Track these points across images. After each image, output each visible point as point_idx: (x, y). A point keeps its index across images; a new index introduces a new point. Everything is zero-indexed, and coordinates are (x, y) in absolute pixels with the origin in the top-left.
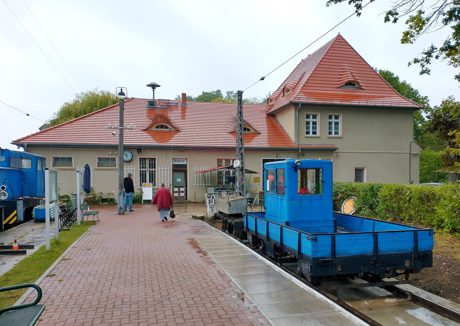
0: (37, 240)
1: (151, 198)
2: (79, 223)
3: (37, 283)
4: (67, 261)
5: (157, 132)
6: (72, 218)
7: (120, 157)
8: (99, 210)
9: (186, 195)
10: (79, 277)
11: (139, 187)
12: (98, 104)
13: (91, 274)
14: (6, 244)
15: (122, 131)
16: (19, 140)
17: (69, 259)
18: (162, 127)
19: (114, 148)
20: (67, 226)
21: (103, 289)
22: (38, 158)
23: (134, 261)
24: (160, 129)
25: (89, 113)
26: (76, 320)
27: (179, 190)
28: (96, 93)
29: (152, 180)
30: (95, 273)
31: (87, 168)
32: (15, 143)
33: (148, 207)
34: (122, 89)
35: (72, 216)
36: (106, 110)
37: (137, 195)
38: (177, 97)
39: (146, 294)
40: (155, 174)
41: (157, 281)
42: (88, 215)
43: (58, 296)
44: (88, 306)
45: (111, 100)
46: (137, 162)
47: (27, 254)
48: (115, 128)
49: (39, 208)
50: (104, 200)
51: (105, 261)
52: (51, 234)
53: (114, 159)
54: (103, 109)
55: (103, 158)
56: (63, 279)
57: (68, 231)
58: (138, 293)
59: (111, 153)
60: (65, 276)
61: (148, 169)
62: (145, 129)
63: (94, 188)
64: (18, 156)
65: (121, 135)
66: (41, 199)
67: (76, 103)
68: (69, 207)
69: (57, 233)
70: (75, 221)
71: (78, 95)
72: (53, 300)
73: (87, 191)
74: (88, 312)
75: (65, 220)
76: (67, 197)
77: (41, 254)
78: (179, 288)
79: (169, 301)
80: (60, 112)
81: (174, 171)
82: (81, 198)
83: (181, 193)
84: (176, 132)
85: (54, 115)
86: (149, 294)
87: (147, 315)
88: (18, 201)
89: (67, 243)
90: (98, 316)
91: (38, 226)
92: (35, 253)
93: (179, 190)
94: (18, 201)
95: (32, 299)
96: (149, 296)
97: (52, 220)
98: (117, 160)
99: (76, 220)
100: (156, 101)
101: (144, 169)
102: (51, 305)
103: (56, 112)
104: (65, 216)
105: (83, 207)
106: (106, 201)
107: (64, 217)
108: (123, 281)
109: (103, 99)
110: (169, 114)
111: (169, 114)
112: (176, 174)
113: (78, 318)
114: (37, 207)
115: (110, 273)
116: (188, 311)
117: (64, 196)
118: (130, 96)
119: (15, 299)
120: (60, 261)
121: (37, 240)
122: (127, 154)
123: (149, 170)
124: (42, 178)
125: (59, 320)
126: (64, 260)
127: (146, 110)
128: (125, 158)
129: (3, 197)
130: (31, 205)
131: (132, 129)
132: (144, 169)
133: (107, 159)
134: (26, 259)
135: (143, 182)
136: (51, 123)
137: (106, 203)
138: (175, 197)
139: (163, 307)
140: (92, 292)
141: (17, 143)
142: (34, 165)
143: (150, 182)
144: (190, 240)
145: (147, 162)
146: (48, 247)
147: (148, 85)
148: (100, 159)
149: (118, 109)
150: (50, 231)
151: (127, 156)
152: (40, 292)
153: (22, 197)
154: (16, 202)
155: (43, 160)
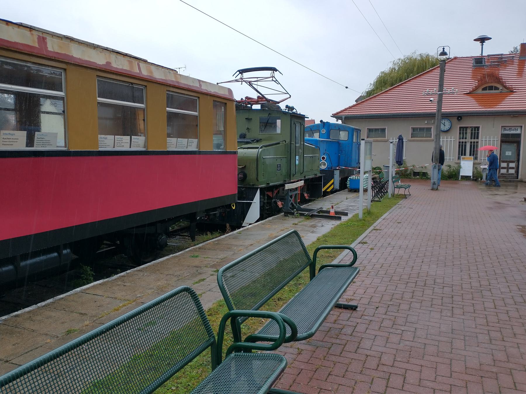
0: (350, 208)
1: (470, 174)
2: (390, 196)
3: (352, 246)
4: (378, 231)
5: (483, 95)
6: (383, 190)
7: (437, 126)
8: (410, 184)
9: (517, 172)
10: (389, 249)
11: (457, 161)
12: (415, 69)
13: (387, 259)
14: (324, 209)
15: (440, 97)
16: (338, 113)
17: (380, 230)
18: (491, 88)
19: (431, 116)
20: (378, 197)
21: (413, 265)
22: (353, 129)
23: (448, 241)
24: (487, 91)
25: (405, 79)
26: (386, 289)
27: (508, 165)
28: (414, 57)
29: (474, 152)
30: (405, 247)
31: (401, 139)
32: (334, 116)
33: (466, 184)
34: (444, 49)
35: (384, 188)
36: (424, 74)
37: (453, 169)
38: (512, 50)
39: (461, 279)
40: (477, 146)
41: (476, 268)
42: (400, 188)
43: (370, 263)
44: (398, 278)
45: (430, 63)
46: (456, 132)
47: (342, 220)
48: (433, 94)
49: (353, 178)
50: (416, 174)
51: (416, 237)
52: (364, 204)
53: (429, 129)
54: (421, 74)
55: (417, 129)
56: (374, 248)
57: (379, 202)
58: (453, 276)
59: (426, 122)
60: (376, 245)
61: (469, 140)
62: (469, 92)
63: (406, 161)
64: (337, 128)
65: (440, 102)
66: (355, 170)
67: (392, 71)
68: (380, 179)
69: (369, 203)
70: (386, 193)
71: (395, 62)
72: (365, 266)
73: (399, 163)
74: (399, 285)
75: (377, 192)
76: (379, 168)
77: (354, 222)
78: (504, 280)
79: (489, 292)
80: (376, 83)
81: (502, 142)
82: (392, 171)
83: (510, 170)
84: (509, 93)
85: (370, 86)
86: (466, 280)
87: (463, 302)
88: (335, 171)
89: (378, 214)
90: (409, 291)
91: (352, 195)
92: (349, 220)
93: (508, 165)
94: (335, 171)
95: (346, 261)
96: (465, 282)
97: (365, 190)
98: (432, 130)
99: (387, 192)
100: (485, 57)
101: (464, 140)
102: (363, 270)
103: (372, 83)
104: (377, 187)
105: (395, 180)
106: (418, 175)
107: (375, 188)
108: (436, 260)
109: (420, 63)
110: (500, 72)
111: (500, 72)
112: (505, 146)
113: (388, 288)
114: (352, 177)
115: (421, 249)
116: (515, 309)
117: (376, 168)
118: (452, 56)
119: (332, 259)
120: (372, 230)
121: (350, 208)
122: (444, 123)
123: (470, 140)
124: (357, 149)
125: (370, 286)
126: (375, 230)
127: (471, 70)
128: (443, 128)
129: (323, 166)
130: (346, 175)
131: (453, 93)
132: (464, 140)
133: (421, 129)
134: (341, 224)
135: (462, 155)
136: (367, 94)
137: (418, 177)
138: (502, 174)
139: (483, 297)
140: (402, 266)
141: (336, 116)
142: (351, 136)
143: (470, 155)
144: (521, 227)
145: (469, 131)
146: (361, 216)
147: (475, 40)
148: (414, 129)
149: (437, 72)
150: (364, 201)
151: (445, 126)
152: (283, 330)
153: (339, 167)
154: (334, 172)
155: (359, 131)
